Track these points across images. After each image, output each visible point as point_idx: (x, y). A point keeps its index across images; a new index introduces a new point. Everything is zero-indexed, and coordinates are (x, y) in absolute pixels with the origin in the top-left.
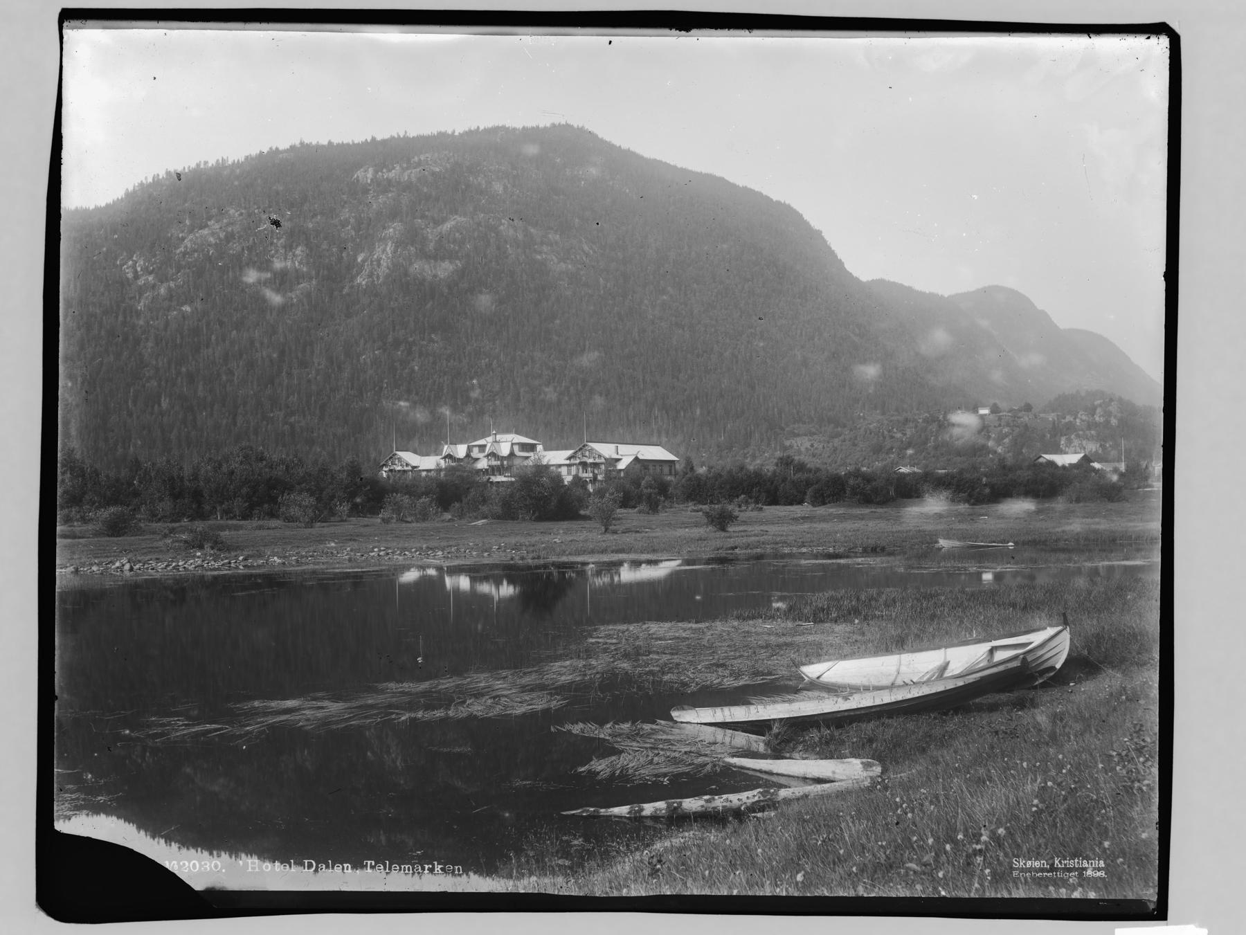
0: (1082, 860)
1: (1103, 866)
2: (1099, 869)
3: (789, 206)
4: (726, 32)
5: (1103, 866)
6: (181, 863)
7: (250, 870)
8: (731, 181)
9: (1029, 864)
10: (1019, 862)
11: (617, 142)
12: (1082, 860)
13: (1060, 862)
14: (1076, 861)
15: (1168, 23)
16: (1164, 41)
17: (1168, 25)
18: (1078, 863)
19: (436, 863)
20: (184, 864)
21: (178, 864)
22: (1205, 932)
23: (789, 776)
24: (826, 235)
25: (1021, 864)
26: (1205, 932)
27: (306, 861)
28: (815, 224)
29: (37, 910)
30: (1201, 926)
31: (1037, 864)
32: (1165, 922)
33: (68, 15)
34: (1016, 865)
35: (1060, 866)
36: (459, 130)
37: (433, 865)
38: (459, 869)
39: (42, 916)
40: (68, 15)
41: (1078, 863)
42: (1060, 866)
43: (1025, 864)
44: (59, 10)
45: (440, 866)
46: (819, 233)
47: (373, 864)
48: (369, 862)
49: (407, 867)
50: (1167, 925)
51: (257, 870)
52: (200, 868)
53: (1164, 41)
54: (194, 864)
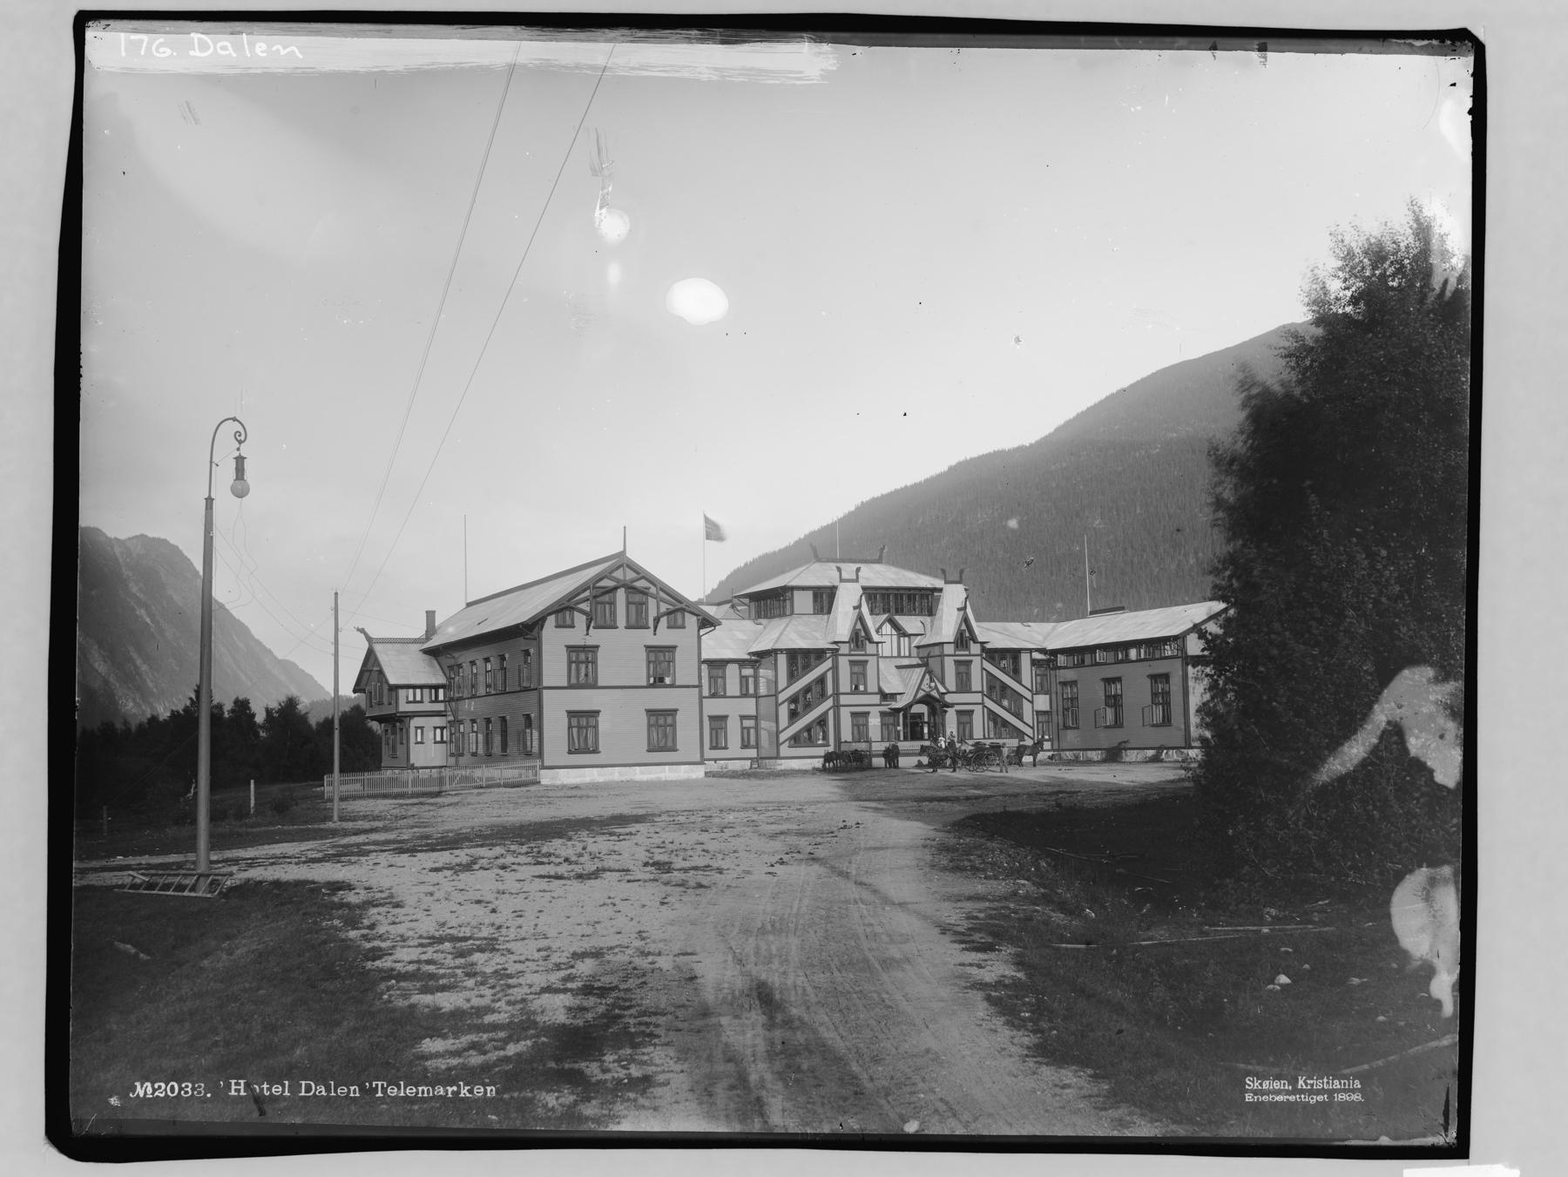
0: (1333, 1080)
1: (1359, 1086)
2: (1354, 1091)
5: (1359, 1086)
6: (196, 1086)
7: (233, 1093)
10: (1253, 1082)
12: (1333, 1080)
13: (1305, 1082)
14: (1325, 1080)
15: (1469, 29)
16: (1460, 67)
17: (1469, 32)
19: (461, 1083)
20: (160, 1087)
21: (153, 1087)
22: (1516, 1173)
23: (442, 669)
25: (1256, 1084)
26: (1516, 1173)
27: (303, 1083)
29: (47, 1146)
30: (1512, 1166)
31: (1277, 1085)
32: (1465, 1161)
34: (1250, 1085)
35: (1304, 1087)
37: (459, 1087)
38: (355, 1090)
39: (53, 1153)
41: (1328, 1083)
42: (1304, 1087)
43: (1261, 1084)
44: (74, 13)
45: (467, 1088)
47: (385, 1086)
48: (380, 1083)
49: (426, 1089)
50: (1469, 1164)
52: (179, 1092)
53: (1460, 67)
54: (172, 1087)
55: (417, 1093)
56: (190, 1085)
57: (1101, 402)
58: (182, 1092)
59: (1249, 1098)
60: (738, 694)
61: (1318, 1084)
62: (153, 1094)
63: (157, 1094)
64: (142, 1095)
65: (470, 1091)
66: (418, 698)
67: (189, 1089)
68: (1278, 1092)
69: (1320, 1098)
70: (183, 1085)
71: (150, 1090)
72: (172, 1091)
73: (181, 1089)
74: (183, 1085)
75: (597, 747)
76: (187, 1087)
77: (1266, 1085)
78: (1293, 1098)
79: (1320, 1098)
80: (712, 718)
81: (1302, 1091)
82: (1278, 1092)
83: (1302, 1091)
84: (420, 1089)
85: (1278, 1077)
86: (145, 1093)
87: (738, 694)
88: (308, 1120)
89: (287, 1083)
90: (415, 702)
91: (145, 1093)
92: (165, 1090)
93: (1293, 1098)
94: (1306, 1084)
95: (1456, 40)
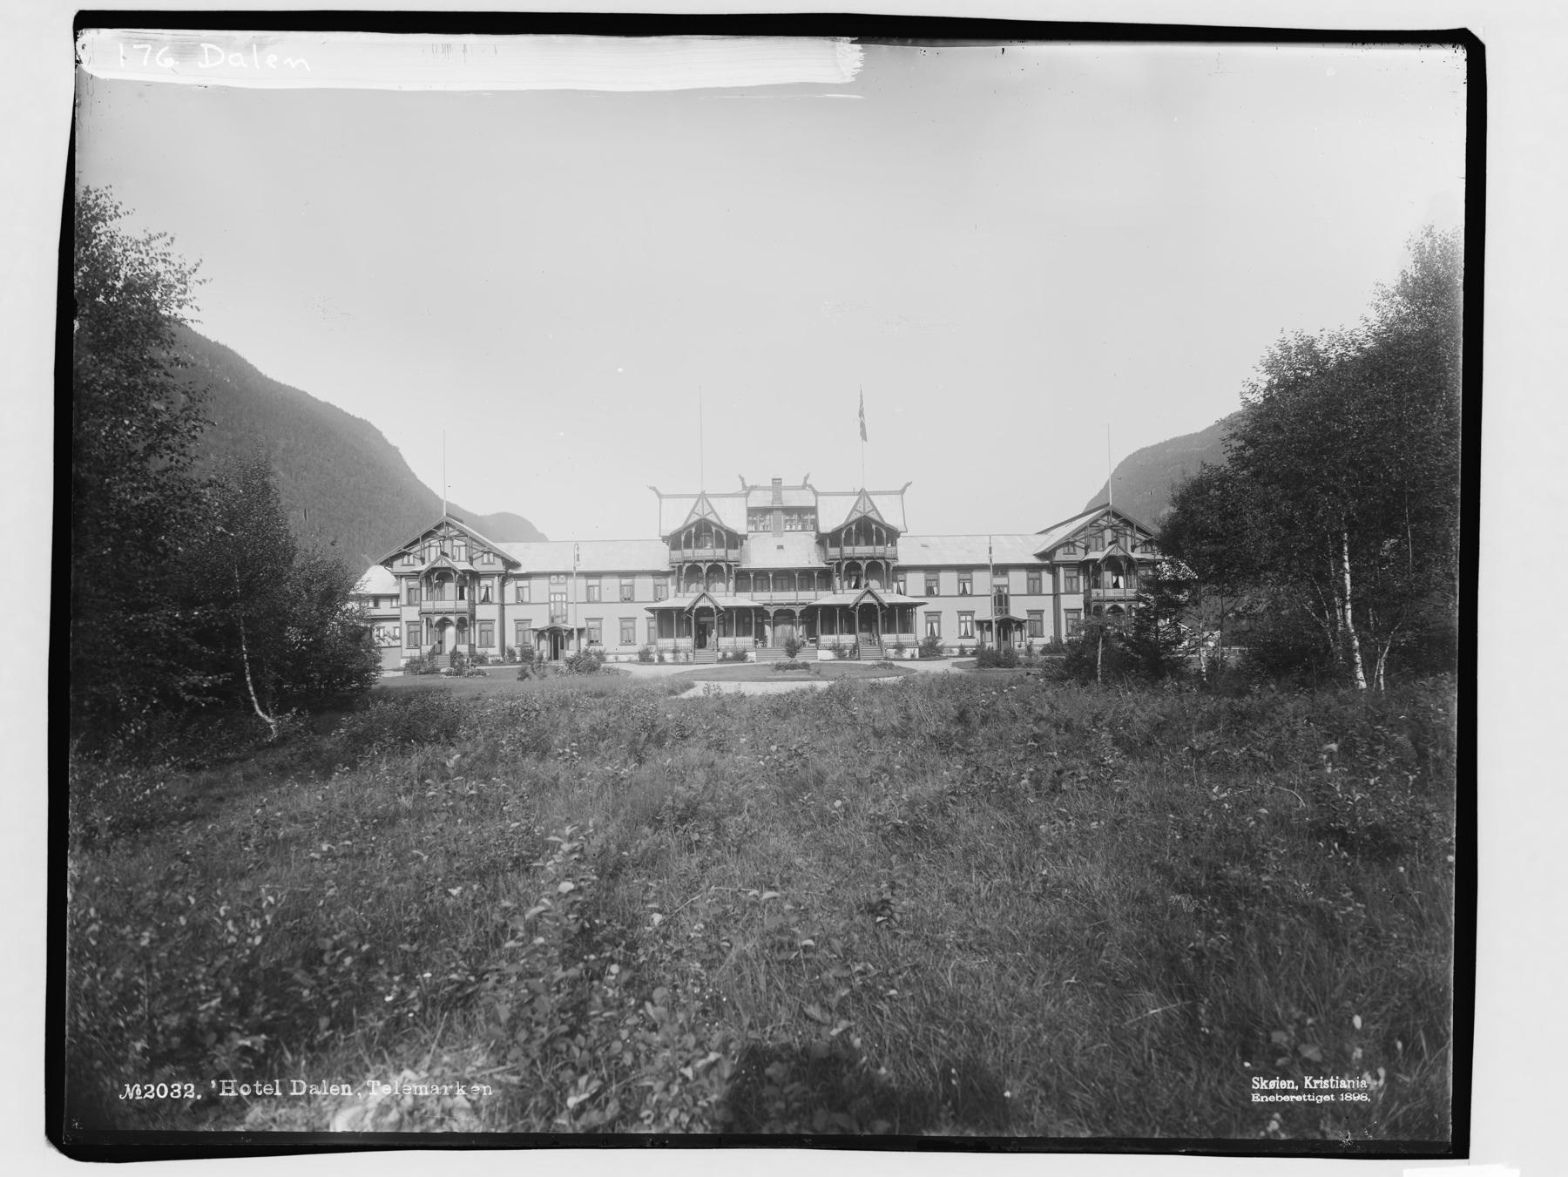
3: (369, 423)
4: (1378, 45)
8: (313, 395)
9: (1272, 1084)
11: (260, 370)
14: (1332, 1080)
15: (1469, 29)
16: (1456, 58)
18: (1334, 1083)
20: (149, 1089)
21: (142, 1088)
22: (1517, 1172)
24: (401, 451)
26: (1517, 1172)
28: (392, 439)
31: (1284, 1084)
33: (86, 20)
36: (323, 400)
40: (86, 20)
42: (1311, 1087)
43: (1267, 1085)
46: (396, 449)
51: (224, 1082)
52: (169, 1094)
53: (1456, 58)
54: (162, 1088)
55: (341, 1091)
56: (179, 1087)
57: (347, 414)
58: (172, 1094)
59: (1256, 1098)
60: (1026, 593)
61: (1325, 1084)
62: (143, 1095)
63: (146, 1095)
64: (131, 1097)
65: (1267, 1085)
66: (411, 562)
67: (178, 1091)
68: (1286, 1092)
69: (1327, 1098)
70: (172, 1087)
71: (139, 1092)
72: (162, 1088)
73: (170, 1090)
74: (172, 1087)
75: (1042, 632)
76: (176, 1088)
77: (1272, 1084)
78: (1299, 1098)
79: (1327, 1098)
80: (1067, 611)
81: (1309, 1091)
82: (1286, 1092)
83: (1309, 1091)
84: (233, 1094)
85: (1285, 1077)
86: (135, 1095)
87: (1026, 593)
88: (511, 1130)
89: (277, 1081)
90: (489, 563)
91: (135, 1095)
92: (155, 1092)
93: (1299, 1098)
94: (1313, 1084)
95: (1461, 38)
